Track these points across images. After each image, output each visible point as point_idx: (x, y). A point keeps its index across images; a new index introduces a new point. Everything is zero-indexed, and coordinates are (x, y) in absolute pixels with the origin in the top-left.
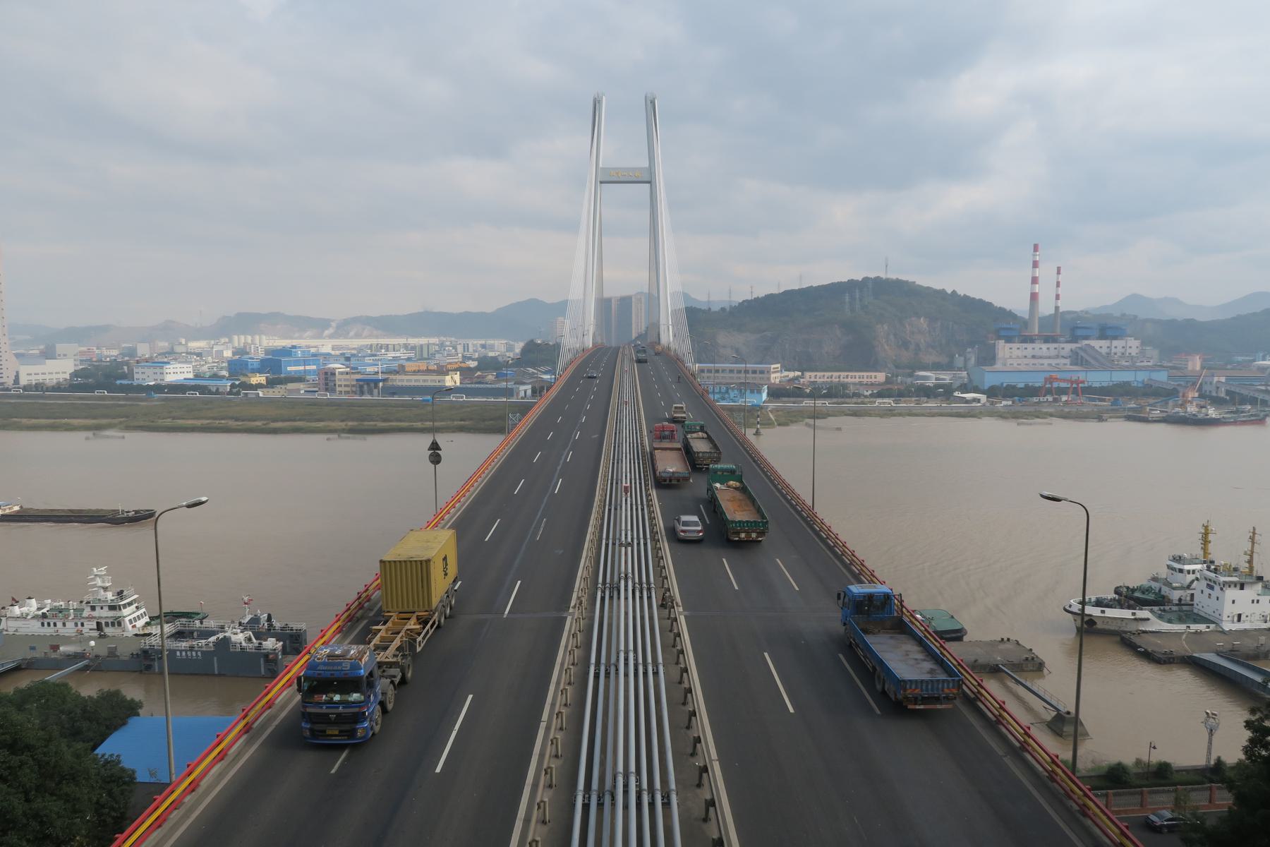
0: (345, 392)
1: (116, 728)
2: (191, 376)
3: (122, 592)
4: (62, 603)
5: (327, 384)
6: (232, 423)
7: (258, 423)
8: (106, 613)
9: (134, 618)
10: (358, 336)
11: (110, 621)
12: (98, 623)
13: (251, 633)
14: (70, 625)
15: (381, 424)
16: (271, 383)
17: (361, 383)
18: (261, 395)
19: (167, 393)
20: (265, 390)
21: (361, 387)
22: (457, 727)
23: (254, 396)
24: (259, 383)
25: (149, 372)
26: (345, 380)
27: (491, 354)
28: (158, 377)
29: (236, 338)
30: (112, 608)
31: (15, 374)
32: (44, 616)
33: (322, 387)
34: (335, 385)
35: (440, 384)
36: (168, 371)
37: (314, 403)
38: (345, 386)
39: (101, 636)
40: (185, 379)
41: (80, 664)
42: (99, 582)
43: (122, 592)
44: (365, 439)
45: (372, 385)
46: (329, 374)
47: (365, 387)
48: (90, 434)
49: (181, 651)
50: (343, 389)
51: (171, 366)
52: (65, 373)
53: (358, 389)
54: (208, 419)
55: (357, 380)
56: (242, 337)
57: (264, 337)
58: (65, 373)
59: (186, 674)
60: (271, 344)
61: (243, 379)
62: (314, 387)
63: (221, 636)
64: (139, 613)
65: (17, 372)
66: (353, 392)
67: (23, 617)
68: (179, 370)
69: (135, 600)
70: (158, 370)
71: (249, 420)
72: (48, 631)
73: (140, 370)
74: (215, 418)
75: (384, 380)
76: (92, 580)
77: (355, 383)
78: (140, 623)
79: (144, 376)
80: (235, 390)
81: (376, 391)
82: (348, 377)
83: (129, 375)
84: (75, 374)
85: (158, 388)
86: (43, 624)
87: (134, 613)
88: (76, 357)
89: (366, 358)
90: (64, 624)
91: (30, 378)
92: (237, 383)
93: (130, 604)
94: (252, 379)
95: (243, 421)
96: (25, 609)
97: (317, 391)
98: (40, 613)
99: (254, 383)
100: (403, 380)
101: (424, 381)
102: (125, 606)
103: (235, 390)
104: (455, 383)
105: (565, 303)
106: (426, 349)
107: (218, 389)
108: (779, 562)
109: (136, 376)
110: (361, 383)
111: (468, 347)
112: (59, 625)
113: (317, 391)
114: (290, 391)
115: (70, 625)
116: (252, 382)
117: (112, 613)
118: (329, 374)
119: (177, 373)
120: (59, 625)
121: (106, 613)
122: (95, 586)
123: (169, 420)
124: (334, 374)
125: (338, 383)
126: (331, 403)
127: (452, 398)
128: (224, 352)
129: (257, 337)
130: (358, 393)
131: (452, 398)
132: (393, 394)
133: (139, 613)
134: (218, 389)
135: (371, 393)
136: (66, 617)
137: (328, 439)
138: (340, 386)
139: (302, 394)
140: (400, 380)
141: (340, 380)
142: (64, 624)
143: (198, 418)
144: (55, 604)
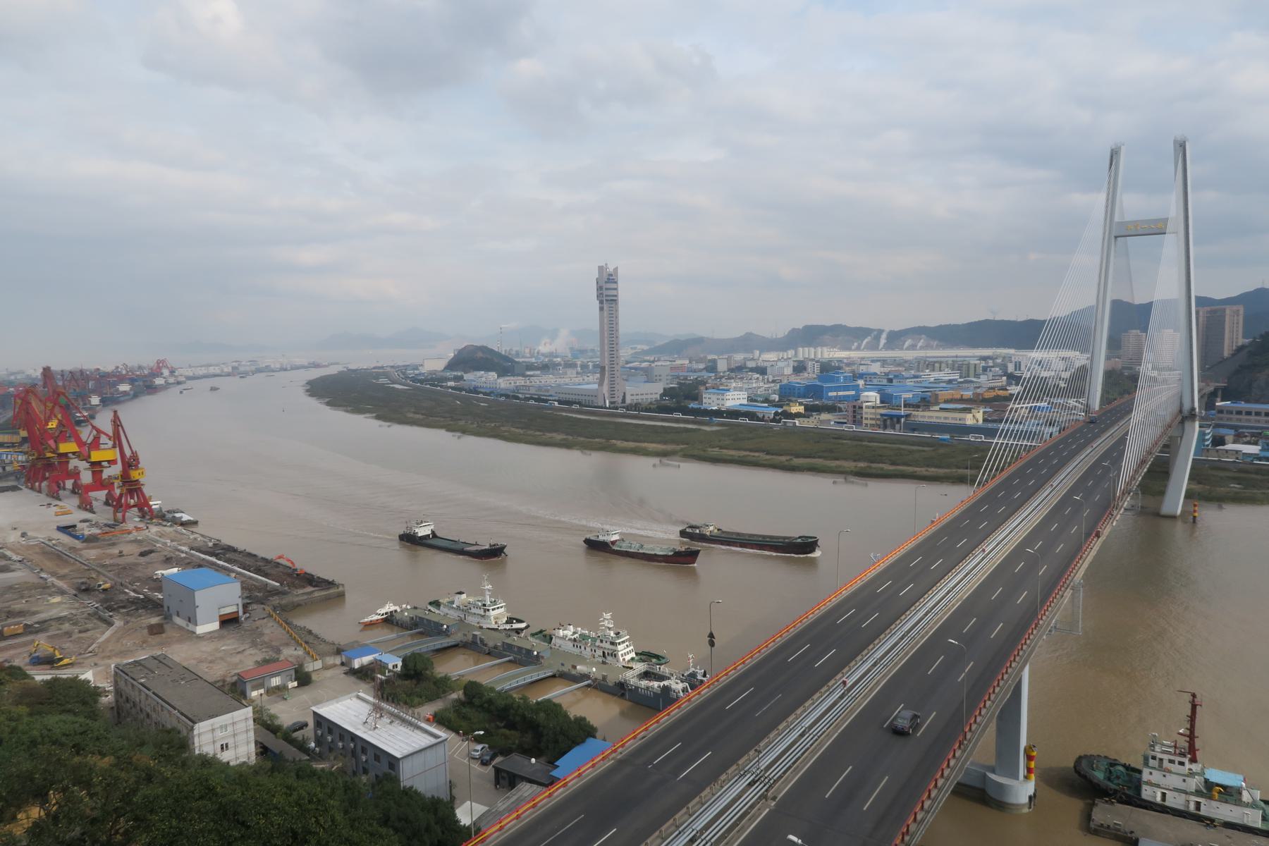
0: (870, 424)
1: (578, 744)
2: (745, 402)
3: (619, 633)
4: (587, 632)
5: (855, 417)
6: (762, 456)
7: (783, 458)
8: (608, 646)
9: (625, 653)
10: (913, 347)
11: (610, 652)
12: (604, 653)
13: (687, 684)
14: (588, 649)
15: (887, 467)
16: (810, 410)
17: (885, 418)
18: (797, 424)
19: (724, 418)
20: (801, 419)
21: (885, 421)
22: (872, 799)
23: (791, 425)
24: (798, 412)
25: (714, 397)
26: (871, 413)
27: (1045, 374)
28: (720, 402)
29: (800, 349)
30: (612, 643)
31: (623, 394)
32: (575, 640)
33: (851, 419)
34: (862, 418)
35: (961, 422)
36: (728, 397)
37: (839, 436)
38: (871, 419)
39: (604, 663)
40: (740, 405)
41: (586, 683)
42: (606, 623)
43: (619, 633)
44: (866, 485)
45: (895, 420)
46: (857, 407)
47: (888, 422)
48: (656, 460)
49: (641, 689)
50: (869, 422)
51: (730, 394)
52: (657, 393)
53: (882, 423)
54: (745, 450)
55: (882, 415)
56: (812, 350)
57: (825, 349)
58: (657, 393)
59: (642, 705)
60: (831, 356)
61: (785, 408)
62: (844, 419)
63: (666, 683)
64: (628, 650)
65: (624, 393)
66: (877, 425)
67: (564, 638)
68: (736, 397)
69: (627, 640)
70: (720, 397)
71: (776, 454)
72: (577, 651)
73: (707, 396)
74: (751, 451)
75: (907, 416)
76: (603, 621)
77: (879, 417)
78: (628, 657)
79: (710, 401)
80: (778, 418)
81: (897, 426)
82: (873, 411)
83: (697, 398)
84: (667, 392)
85: (718, 413)
86: (574, 646)
87: (625, 649)
88: (668, 378)
89: (908, 380)
90: (585, 649)
91: (633, 397)
92: (780, 411)
93: (623, 642)
94: (792, 408)
95: (772, 454)
96: (565, 632)
97: (845, 423)
98: (573, 637)
99: (793, 412)
100: (924, 417)
101: (946, 418)
102: (619, 644)
103: (778, 418)
104: (977, 421)
105: (1151, 304)
106: (973, 369)
107: (764, 416)
108: (849, 769)
109: (704, 401)
110: (885, 418)
111: (1020, 365)
112: (583, 648)
113: (845, 423)
114: (822, 422)
115: (588, 649)
116: (792, 411)
117: (611, 647)
118: (857, 407)
119: (735, 399)
120: (583, 648)
121: (608, 646)
122: (603, 625)
123: (717, 449)
124: (861, 408)
125: (864, 416)
126: (856, 438)
127: (971, 438)
128: (785, 369)
129: (819, 350)
130: (882, 426)
131: (971, 438)
132: (914, 430)
133: (628, 650)
134: (764, 416)
135: (894, 428)
136: (586, 644)
137: (834, 482)
138: (866, 419)
139: (832, 426)
140: (922, 417)
141: (866, 413)
142: (585, 649)
143: (739, 449)
144: (584, 632)
